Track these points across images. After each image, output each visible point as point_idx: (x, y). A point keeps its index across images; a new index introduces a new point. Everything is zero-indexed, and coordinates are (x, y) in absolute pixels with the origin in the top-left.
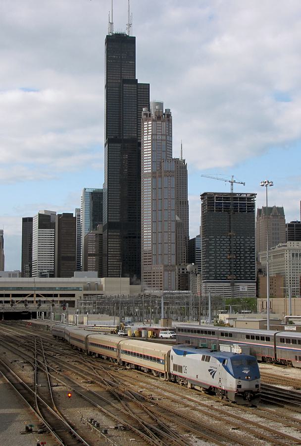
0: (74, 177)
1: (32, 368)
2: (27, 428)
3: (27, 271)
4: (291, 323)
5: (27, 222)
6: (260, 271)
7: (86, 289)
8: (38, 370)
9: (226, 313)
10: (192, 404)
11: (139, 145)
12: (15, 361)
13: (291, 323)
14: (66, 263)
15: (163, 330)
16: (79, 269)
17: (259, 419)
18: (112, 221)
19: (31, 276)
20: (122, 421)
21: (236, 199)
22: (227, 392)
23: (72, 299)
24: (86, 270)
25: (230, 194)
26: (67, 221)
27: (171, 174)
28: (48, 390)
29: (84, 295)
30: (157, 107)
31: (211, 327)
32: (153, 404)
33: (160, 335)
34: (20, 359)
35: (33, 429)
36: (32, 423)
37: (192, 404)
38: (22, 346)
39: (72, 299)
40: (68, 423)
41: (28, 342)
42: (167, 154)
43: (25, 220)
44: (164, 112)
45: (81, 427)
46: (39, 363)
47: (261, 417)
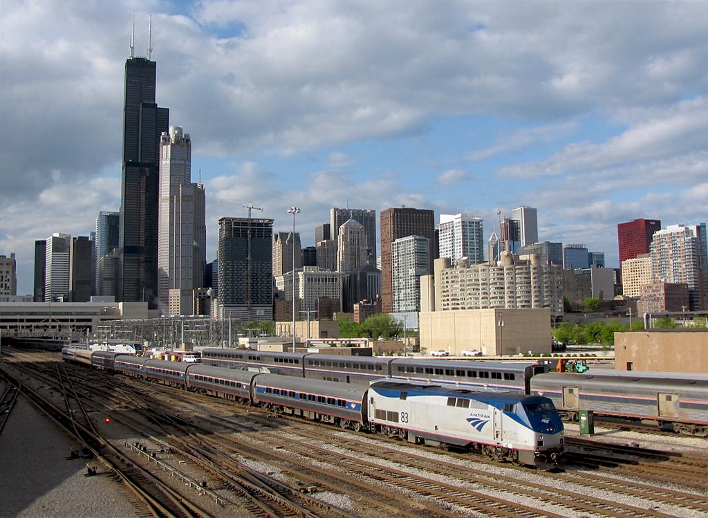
0: (87, 201)
1: (60, 394)
2: (73, 453)
3: (39, 295)
4: (312, 345)
5: (41, 245)
6: (276, 295)
7: (103, 314)
8: (68, 396)
9: (245, 337)
10: (231, 425)
11: (155, 168)
12: (42, 387)
13: (312, 345)
14: (83, 288)
15: (187, 354)
16: (94, 294)
17: (300, 438)
18: (129, 244)
19: (43, 301)
20: (167, 445)
21: (253, 224)
22: (517, 451)
23: (89, 324)
24: (101, 295)
25: (248, 219)
26: (83, 245)
27: (189, 199)
28: (83, 416)
29: (102, 320)
30: (176, 132)
31: (234, 350)
32: (193, 426)
33: (184, 359)
34: (46, 385)
35: (80, 454)
36: (78, 449)
37: (231, 425)
38: (44, 372)
39: (89, 324)
40: (114, 447)
41: (50, 368)
42: (185, 179)
43: (38, 243)
44: (183, 137)
45: (128, 452)
46: (67, 389)
47: (301, 436)
